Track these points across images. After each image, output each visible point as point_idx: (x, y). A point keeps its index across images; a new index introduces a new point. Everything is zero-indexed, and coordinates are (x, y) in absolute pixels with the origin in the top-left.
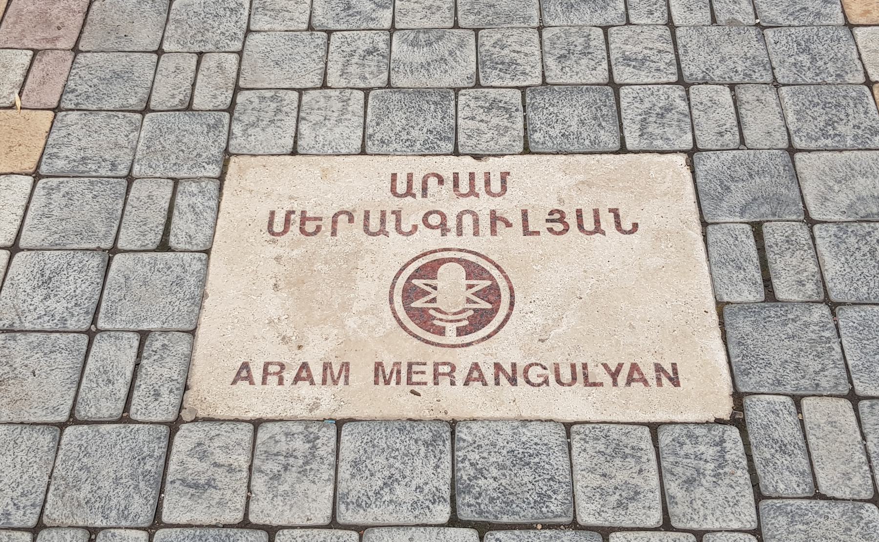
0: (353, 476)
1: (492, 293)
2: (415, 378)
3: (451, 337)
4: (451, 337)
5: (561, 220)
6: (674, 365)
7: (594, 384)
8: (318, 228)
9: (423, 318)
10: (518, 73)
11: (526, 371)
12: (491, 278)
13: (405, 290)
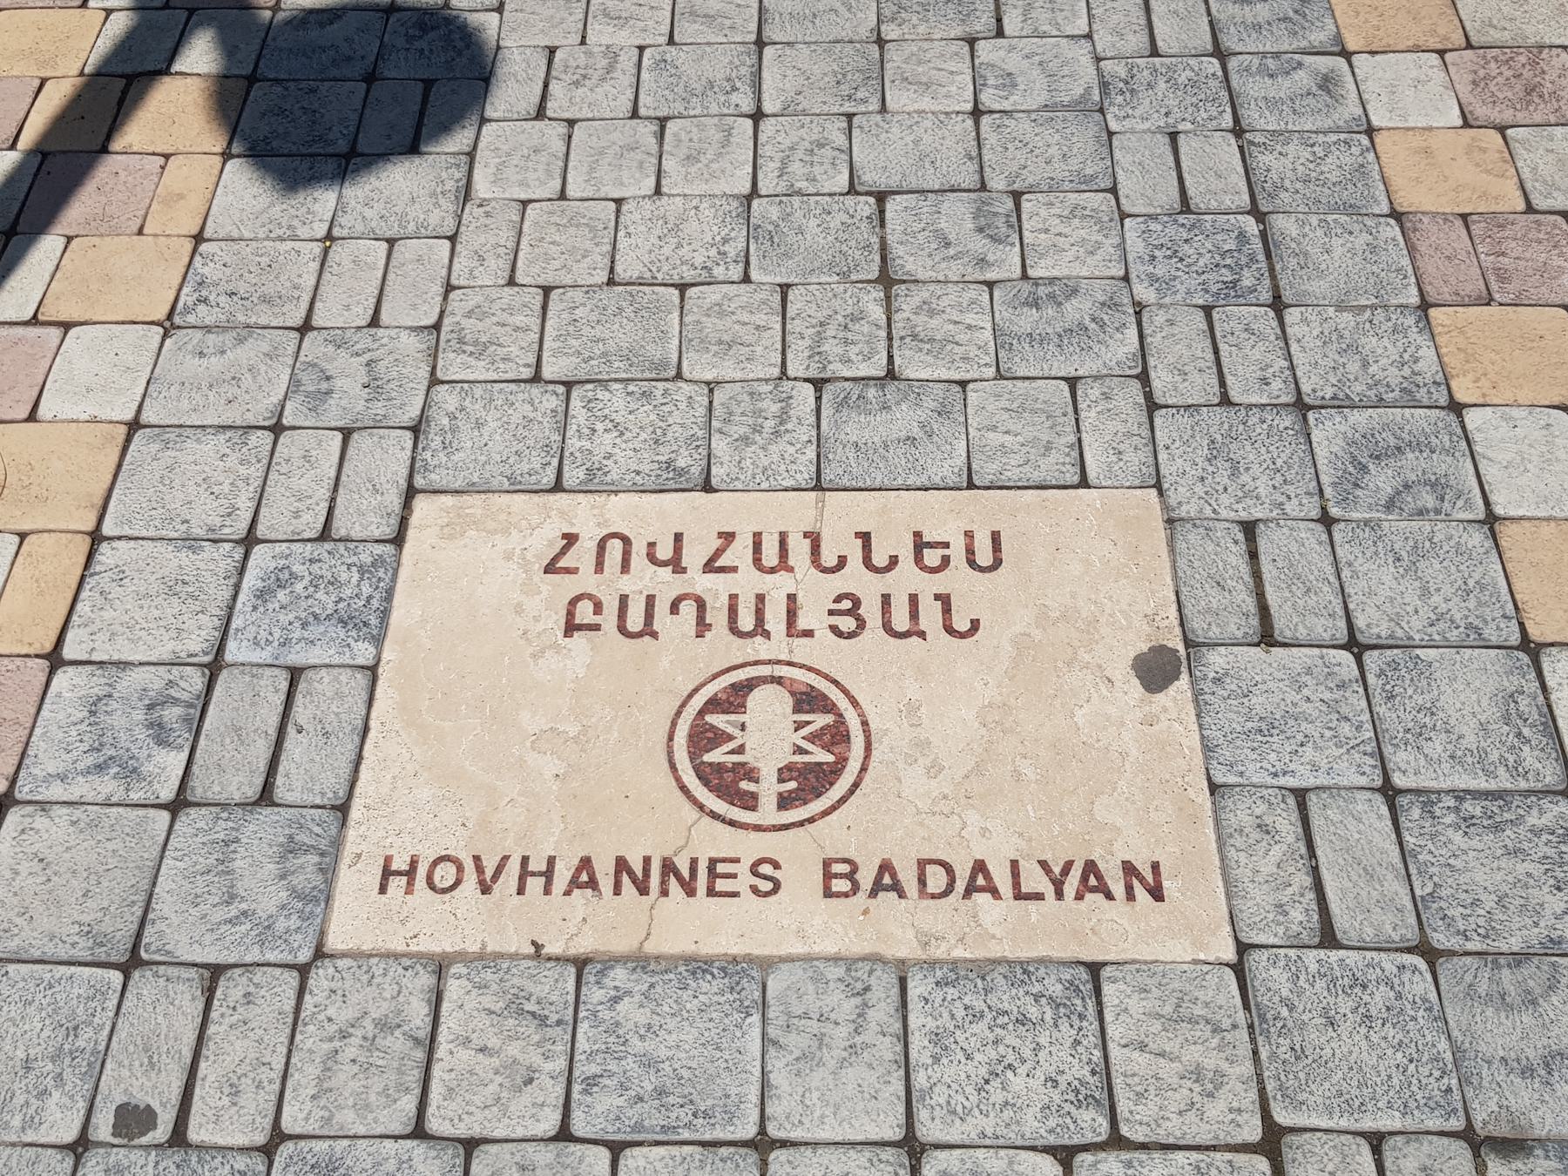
0: (936, 1059)
1: (836, 737)
2: (721, 885)
3: (768, 812)
4: (768, 812)
6: (1155, 867)
8: (946, 560)
9: (730, 783)
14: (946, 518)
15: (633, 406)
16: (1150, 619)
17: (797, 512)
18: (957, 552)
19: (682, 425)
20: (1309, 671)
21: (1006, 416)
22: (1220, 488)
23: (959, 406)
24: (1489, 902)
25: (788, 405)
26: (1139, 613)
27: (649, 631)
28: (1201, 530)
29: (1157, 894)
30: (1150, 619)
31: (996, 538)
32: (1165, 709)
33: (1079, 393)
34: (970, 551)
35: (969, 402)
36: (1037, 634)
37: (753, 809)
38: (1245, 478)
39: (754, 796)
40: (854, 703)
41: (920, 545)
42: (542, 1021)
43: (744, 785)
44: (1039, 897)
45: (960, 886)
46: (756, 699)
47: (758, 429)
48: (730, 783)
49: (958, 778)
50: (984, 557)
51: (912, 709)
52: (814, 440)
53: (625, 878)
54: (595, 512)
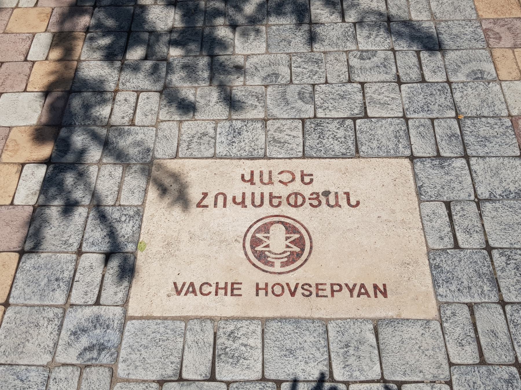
1: (300, 242)
3: (277, 268)
4: (277, 268)
5: (317, 198)
6: (384, 285)
9: (261, 256)
10: (389, 109)
11: (201, 288)
12: (299, 233)
13: (251, 242)
29: (385, 294)
41: (303, 176)
53: (378, 292)
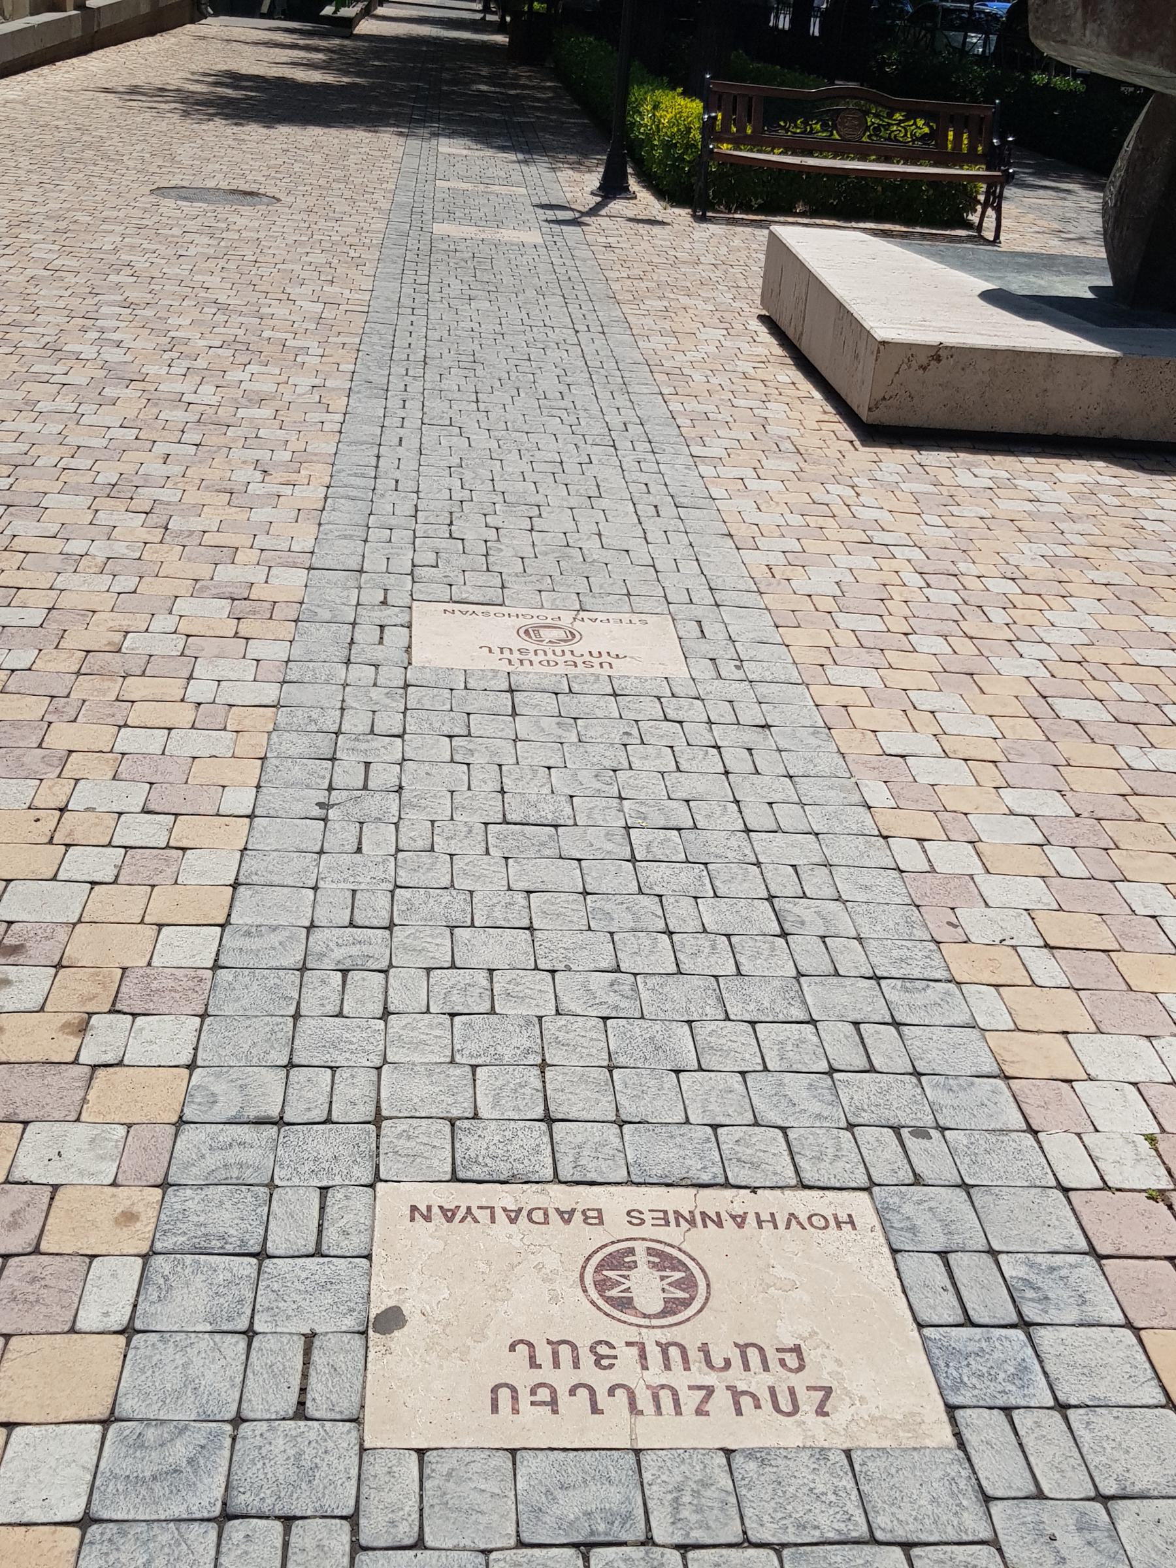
3: (640, 1248)
5: (599, 1359)
6: (412, 1219)
7: (487, 1208)
8: (533, 1392)
9: (663, 1260)
12: (608, 1300)
14: (532, 1426)
15: (810, 1517)
16: (388, 1351)
17: (654, 1431)
18: (525, 1398)
19: (761, 1499)
20: (288, 1317)
21: (483, 1507)
22: (314, 1444)
23: (523, 1518)
24: (228, 1205)
25: (673, 1516)
26: (393, 1356)
27: (743, 1348)
28: (337, 1409)
29: (414, 1208)
30: (388, 1351)
31: (495, 1408)
32: (390, 1297)
33: (416, 1529)
34: (515, 1398)
35: (514, 1526)
36: (469, 1342)
37: (648, 1248)
38: (291, 1452)
39: (649, 1254)
40: (593, 1303)
41: (553, 1403)
42: (739, 1160)
43: (657, 1260)
44: (480, 1208)
45: (524, 1213)
46: (659, 1306)
47: (696, 1494)
48: (663, 1260)
49: (525, 1263)
50: (504, 1395)
51: (555, 1299)
52: (646, 1487)
53: (417, 1214)
54: (809, 1433)
